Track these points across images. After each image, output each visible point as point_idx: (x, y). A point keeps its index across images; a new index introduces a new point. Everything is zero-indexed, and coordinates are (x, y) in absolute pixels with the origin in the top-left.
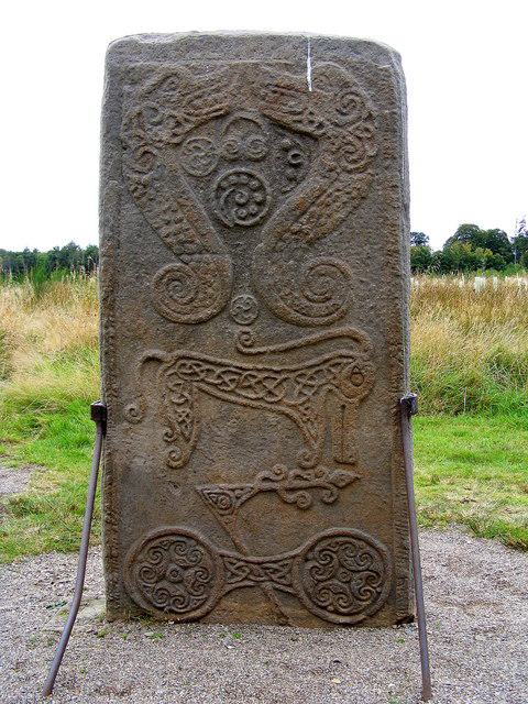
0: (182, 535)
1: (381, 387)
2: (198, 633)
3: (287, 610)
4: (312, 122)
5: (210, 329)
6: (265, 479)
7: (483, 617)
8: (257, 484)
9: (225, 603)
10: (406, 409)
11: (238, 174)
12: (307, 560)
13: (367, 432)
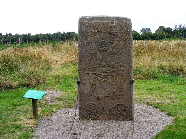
0: (92, 104)
1: (127, 78)
2: (95, 121)
3: (111, 117)
5: (98, 68)
6: (107, 94)
7: (146, 119)
8: (106, 95)
9: (100, 116)
10: (132, 82)
11: (102, 41)
13: (125, 86)
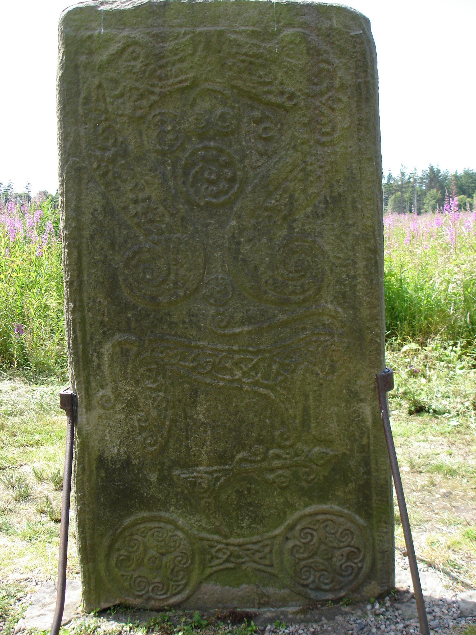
4: (282, 93)
12: (287, 539)
